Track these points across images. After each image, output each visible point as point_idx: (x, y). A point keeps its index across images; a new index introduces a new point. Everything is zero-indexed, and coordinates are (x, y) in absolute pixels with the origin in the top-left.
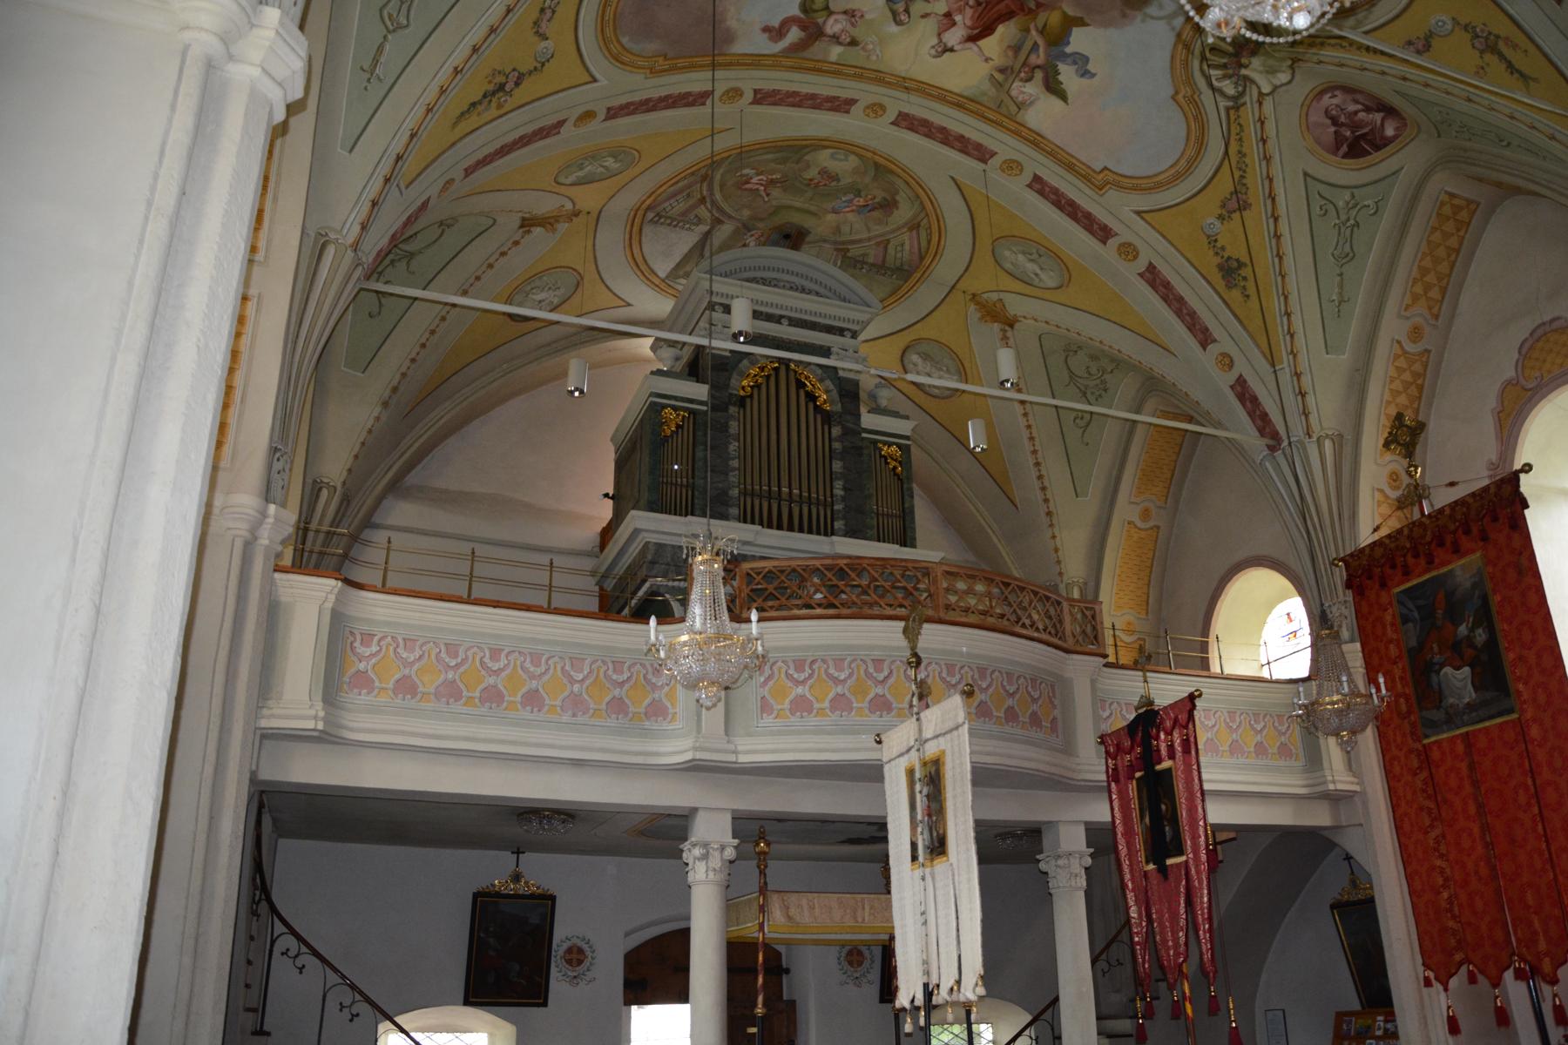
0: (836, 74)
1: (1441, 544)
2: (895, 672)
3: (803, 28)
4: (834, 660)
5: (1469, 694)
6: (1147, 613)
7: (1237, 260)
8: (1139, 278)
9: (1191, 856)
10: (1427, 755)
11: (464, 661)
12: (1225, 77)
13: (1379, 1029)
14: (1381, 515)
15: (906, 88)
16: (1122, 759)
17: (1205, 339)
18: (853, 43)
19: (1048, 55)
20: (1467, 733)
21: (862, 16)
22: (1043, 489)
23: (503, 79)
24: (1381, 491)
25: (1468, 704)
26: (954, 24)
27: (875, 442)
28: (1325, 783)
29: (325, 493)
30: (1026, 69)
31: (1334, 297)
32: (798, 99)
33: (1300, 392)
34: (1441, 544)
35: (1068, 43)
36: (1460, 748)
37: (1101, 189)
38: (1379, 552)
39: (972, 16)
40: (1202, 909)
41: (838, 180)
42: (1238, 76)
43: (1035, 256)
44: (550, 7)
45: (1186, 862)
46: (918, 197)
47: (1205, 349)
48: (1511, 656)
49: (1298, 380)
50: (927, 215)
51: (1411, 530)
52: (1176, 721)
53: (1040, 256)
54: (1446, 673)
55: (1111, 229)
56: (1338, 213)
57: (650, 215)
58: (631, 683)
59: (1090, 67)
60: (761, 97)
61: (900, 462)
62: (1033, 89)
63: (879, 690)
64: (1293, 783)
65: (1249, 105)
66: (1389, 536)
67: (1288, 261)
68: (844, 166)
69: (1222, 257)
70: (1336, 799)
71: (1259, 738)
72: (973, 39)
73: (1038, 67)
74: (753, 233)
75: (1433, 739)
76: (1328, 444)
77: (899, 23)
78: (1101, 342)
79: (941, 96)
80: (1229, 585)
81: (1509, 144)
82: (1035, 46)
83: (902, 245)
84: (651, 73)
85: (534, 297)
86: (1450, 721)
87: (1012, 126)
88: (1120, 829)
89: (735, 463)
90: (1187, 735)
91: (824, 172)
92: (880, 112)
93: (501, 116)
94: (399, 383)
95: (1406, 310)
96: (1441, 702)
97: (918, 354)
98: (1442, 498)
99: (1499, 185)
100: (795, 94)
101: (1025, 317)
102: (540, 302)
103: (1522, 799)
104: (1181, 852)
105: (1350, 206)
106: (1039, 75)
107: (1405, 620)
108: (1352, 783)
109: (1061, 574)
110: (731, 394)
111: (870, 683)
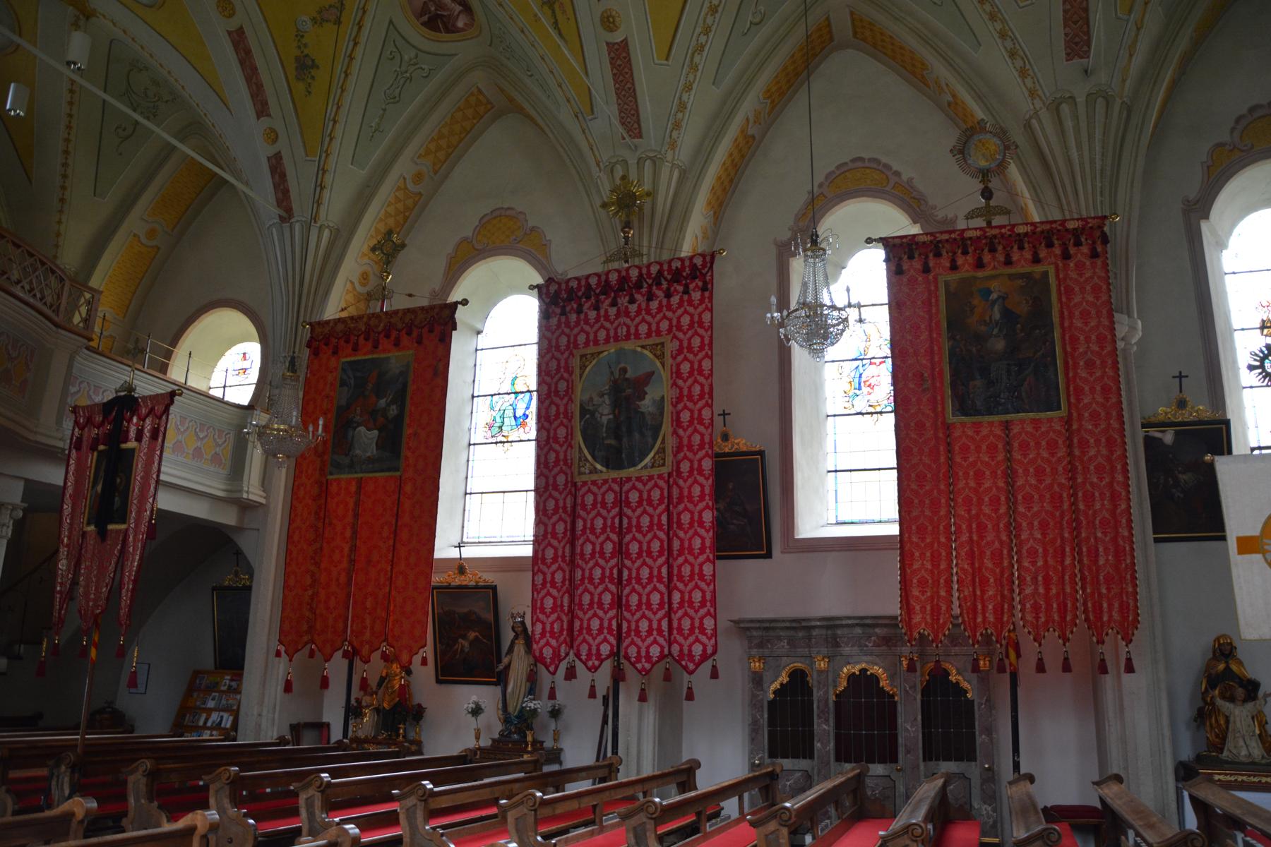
1: (388, 336)
5: (372, 451)
6: (124, 317)
7: (313, 61)
8: (226, 34)
9: (132, 526)
10: (327, 488)
13: (225, 685)
14: (346, 301)
16: (90, 430)
17: (262, 110)
20: (362, 478)
22: (65, 176)
24: (352, 283)
25: (369, 457)
28: (241, 491)
31: (373, 125)
34: (388, 336)
36: (353, 488)
38: (340, 327)
40: (130, 571)
45: (127, 530)
47: (258, 119)
48: (410, 431)
51: (369, 319)
52: (151, 411)
54: (360, 431)
64: (216, 486)
66: (352, 318)
69: (302, 52)
70: (246, 507)
76: (326, 233)
78: (169, 72)
80: (203, 316)
81: (531, 76)
86: (351, 467)
88: (70, 491)
90: (159, 424)
95: (419, 157)
98: (398, 303)
99: (511, 100)
101: (104, 16)
103: (385, 534)
104: (123, 519)
105: (412, 62)
107: (343, 384)
108: (261, 496)
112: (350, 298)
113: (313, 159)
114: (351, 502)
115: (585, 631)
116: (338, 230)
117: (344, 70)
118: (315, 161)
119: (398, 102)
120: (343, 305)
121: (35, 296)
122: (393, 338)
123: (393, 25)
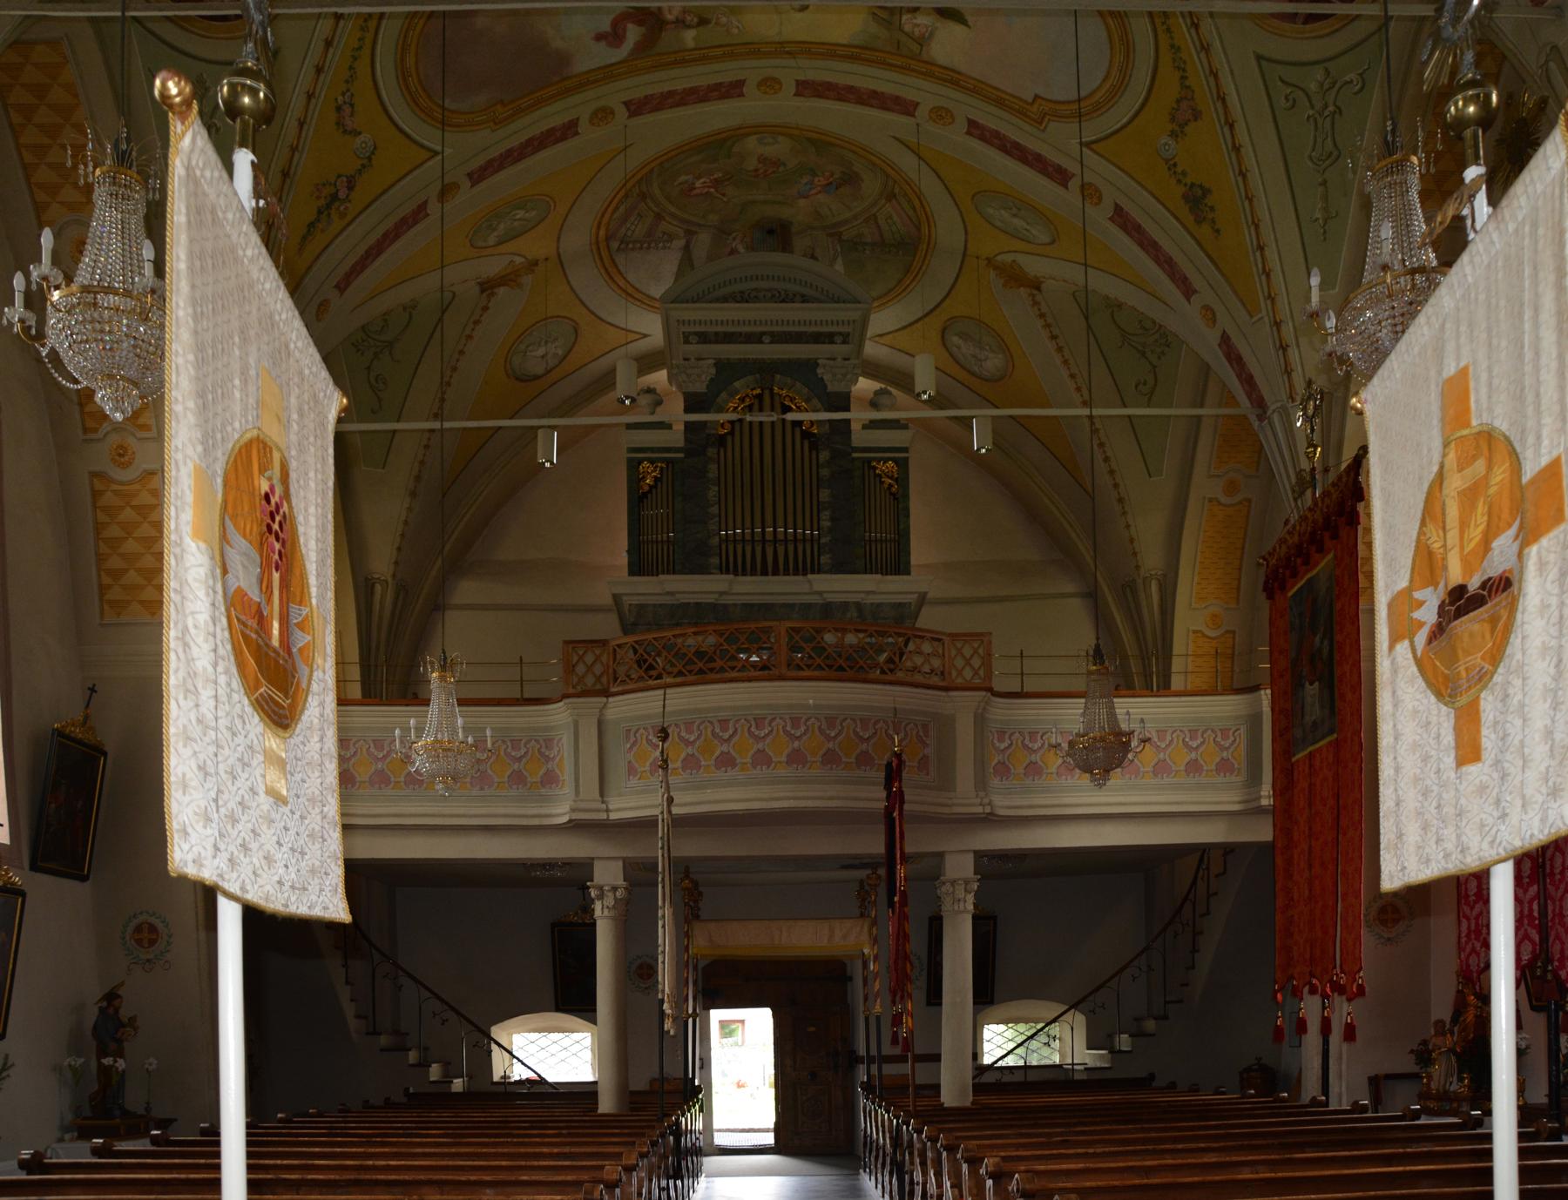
2: (739, 730)
3: (640, 23)
4: (719, 721)
6: (1238, 603)
7: (1201, 186)
11: (389, 753)
15: (788, 53)
17: (1188, 291)
23: (333, 190)
27: (869, 461)
29: (378, 588)
31: (1318, 215)
33: (1281, 346)
37: (1041, 123)
41: (784, 165)
43: (1014, 211)
44: (345, 102)
46: (874, 164)
49: (1279, 331)
50: (895, 182)
53: (1019, 209)
55: (1066, 170)
56: (1310, 101)
57: (615, 245)
58: (528, 757)
60: (636, 108)
61: (896, 480)
63: (725, 748)
68: (779, 148)
69: (1186, 185)
71: (1193, 755)
74: (734, 235)
79: (830, 51)
83: (891, 217)
84: (495, 124)
85: (533, 354)
89: (714, 510)
91: (763, 159)
92: (777, 87)
93: (349, 224)
94: (420, 471)
97: (956, 335)
100: (671, 94)
102: (543, 357)
105: (1326, 86)
108: (1234, 803)
109: (1138, 567)
110: (709, 435)
111: (716, 742)
113: (1260, 316)
115: (1526, 922)
117: (1237, 172)
118: (1262, 318)
119: (1339, 156)
123: (1269, 60)
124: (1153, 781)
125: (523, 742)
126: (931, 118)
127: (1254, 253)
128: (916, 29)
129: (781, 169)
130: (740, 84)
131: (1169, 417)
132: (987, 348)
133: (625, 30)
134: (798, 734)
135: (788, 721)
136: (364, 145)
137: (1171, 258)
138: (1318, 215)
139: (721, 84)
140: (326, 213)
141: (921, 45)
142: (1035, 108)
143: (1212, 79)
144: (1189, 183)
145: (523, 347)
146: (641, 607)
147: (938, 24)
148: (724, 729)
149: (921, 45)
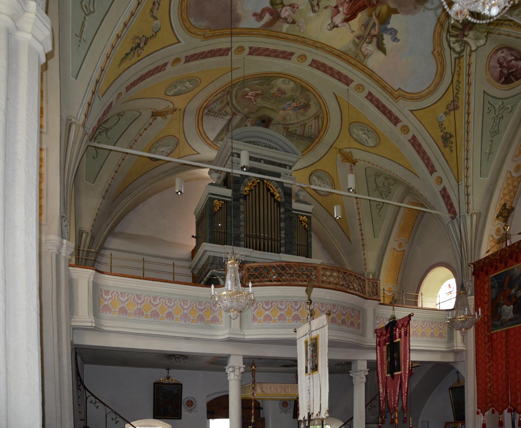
0: (286, 39)
2: (302, 306)
3: (271, 14)
5: (511, 315)
8: (408, 142)
9: (403, 371)
12: (457, 41)
14: (490, 246)
15: (316, 47)
16: (382, 338)
17: (432, 170)
18: (294, 22)
19: (379, 30)
20: (507, 329)
21: (298, 8)
22: (362, 234)
23: (139, 42)
24: (492, 236)
25: (510, 319)
26: (339, 12)
27: (297, 215)
29: (84, 235)
30: (369, 37)
31: (487, 152)
32: (269, 52)
33: (467, 194)
35: (389, 23)
36: (504, 334)
37: (396, 99)
38: (487, 261)
39: (347, 8)
40: (405, 389)
41: (285, 94)
42: (462, 41)
43: (366, 131)
45: (401, 373)
46: (319, 102)
50: (322, 112)
52: (403, 325)
53: (368, 131)
54: (504, 308)
55: (399, 119)
57: (206, 111)
59: (398, 36)
60: (253, 51)
61: (307, 223)
62: (371, 48)
63: (296, 313)
65: (465, 56)
66: (492, 255)
67: (471, 134)
68: (288, 87)
69: (444, 132)
70: (456, 352)
71: (432, 331)
72: (347, 20)
73: (375, 36)
75: (495, 331)
76: (475, 217)
77: (314, 11)
82: (374, 23)
83: (311, 126)
84: (204, 38)
86: (502, 325)
87: (361, 67)
88: (379, 363)
89: (243, 223)
90: (406, 330)
91: (279, 90)
94: (108, 188)
95: (516, 157)
96: (500, 318)
101: (360, 160)
102: (162, 152)
104: (399, 370)
105: (501, 108)
106: (375, 40)
107: (492, 287)
108: (463, 347)
109: (366, 269)
110: (241, 194)
111: (293, 310)
112: (493, 244)
114: (504, 341)
116: (480, 213)
117: (466, 131)
120: (489, 248)
121: (355, 290)
122: (514, 258)
123: (488, 94)
124: (421, 339)
125: (203, 303)
126: (355, 87)
127: (464, 160)
128: (366, 51)
129: (284, 96)
130: (292, 54)
131: (425, 212)
132: (326, 183)
133: (264, 16)
134: (323, 310)
135: (320, 304)
136: (156, 26)
137: (429, 158)
138: (487, 152)
139: (286, 51)
140: (134, 51)
141: (365, 58)
142: (397, 93)
143: (467, 96)
144: (445, 132)
145: (157, 145)
146: (214, 257)
147: (375, 51)
148: (296, 305)
149: (365, 58)
